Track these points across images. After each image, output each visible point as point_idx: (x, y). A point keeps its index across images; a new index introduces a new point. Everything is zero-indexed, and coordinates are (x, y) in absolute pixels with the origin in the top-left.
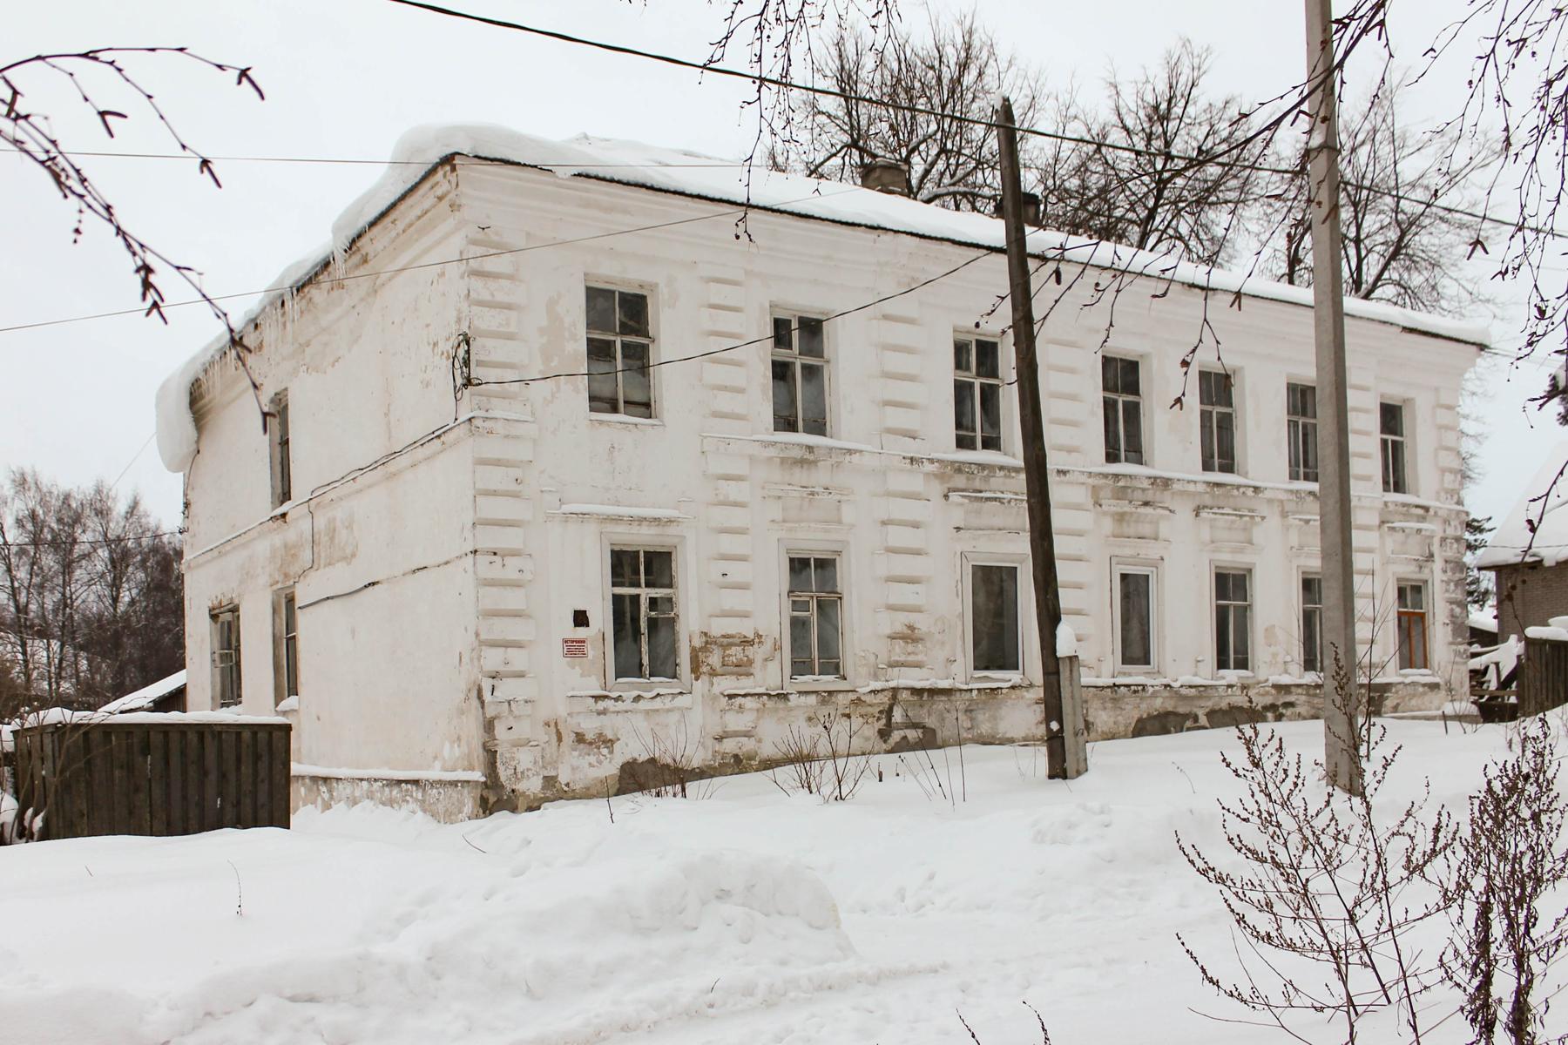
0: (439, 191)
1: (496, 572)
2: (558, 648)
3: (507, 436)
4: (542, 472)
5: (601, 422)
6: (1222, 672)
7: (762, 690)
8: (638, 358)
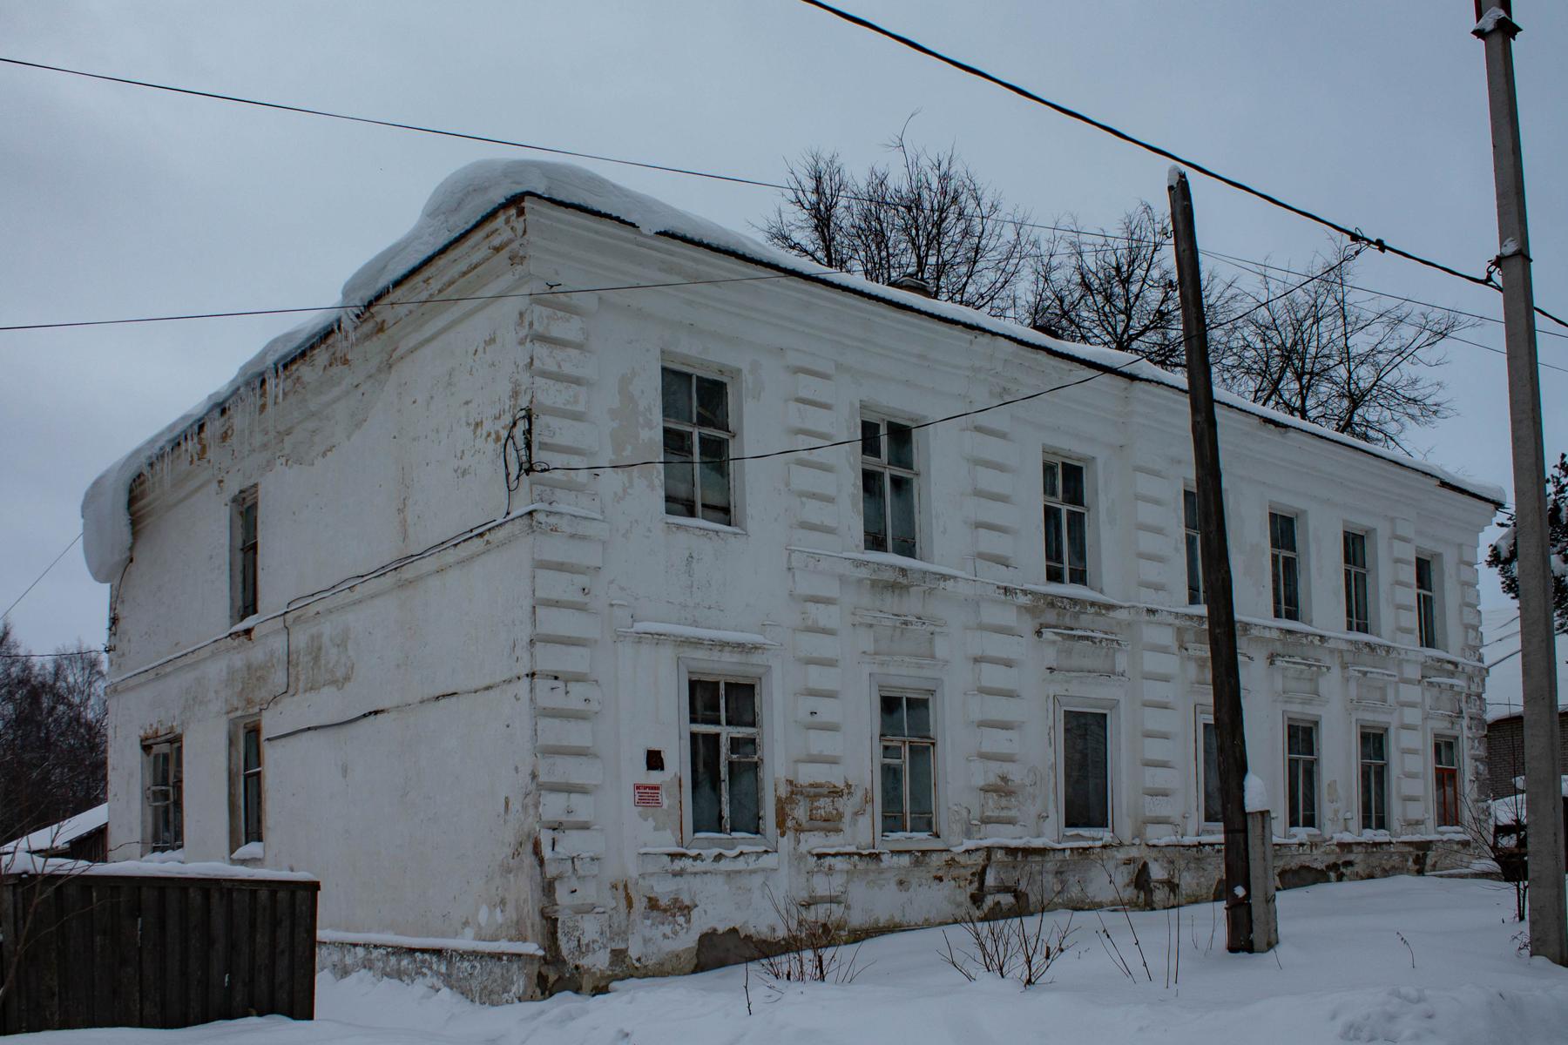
0: (496, 241)
1: (557, 701)
2: (628, 795)
3: (572, 536)
4: (612, 582)
5: (679, 527)
6: (1295, 830)
7: (852, 849)
8: (716, 454)
